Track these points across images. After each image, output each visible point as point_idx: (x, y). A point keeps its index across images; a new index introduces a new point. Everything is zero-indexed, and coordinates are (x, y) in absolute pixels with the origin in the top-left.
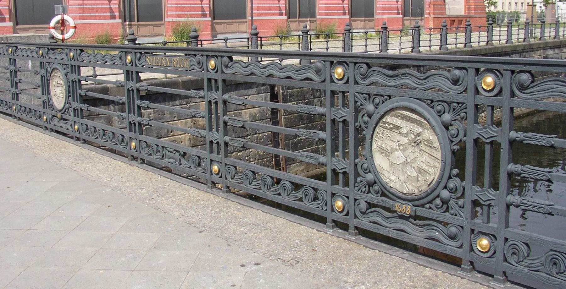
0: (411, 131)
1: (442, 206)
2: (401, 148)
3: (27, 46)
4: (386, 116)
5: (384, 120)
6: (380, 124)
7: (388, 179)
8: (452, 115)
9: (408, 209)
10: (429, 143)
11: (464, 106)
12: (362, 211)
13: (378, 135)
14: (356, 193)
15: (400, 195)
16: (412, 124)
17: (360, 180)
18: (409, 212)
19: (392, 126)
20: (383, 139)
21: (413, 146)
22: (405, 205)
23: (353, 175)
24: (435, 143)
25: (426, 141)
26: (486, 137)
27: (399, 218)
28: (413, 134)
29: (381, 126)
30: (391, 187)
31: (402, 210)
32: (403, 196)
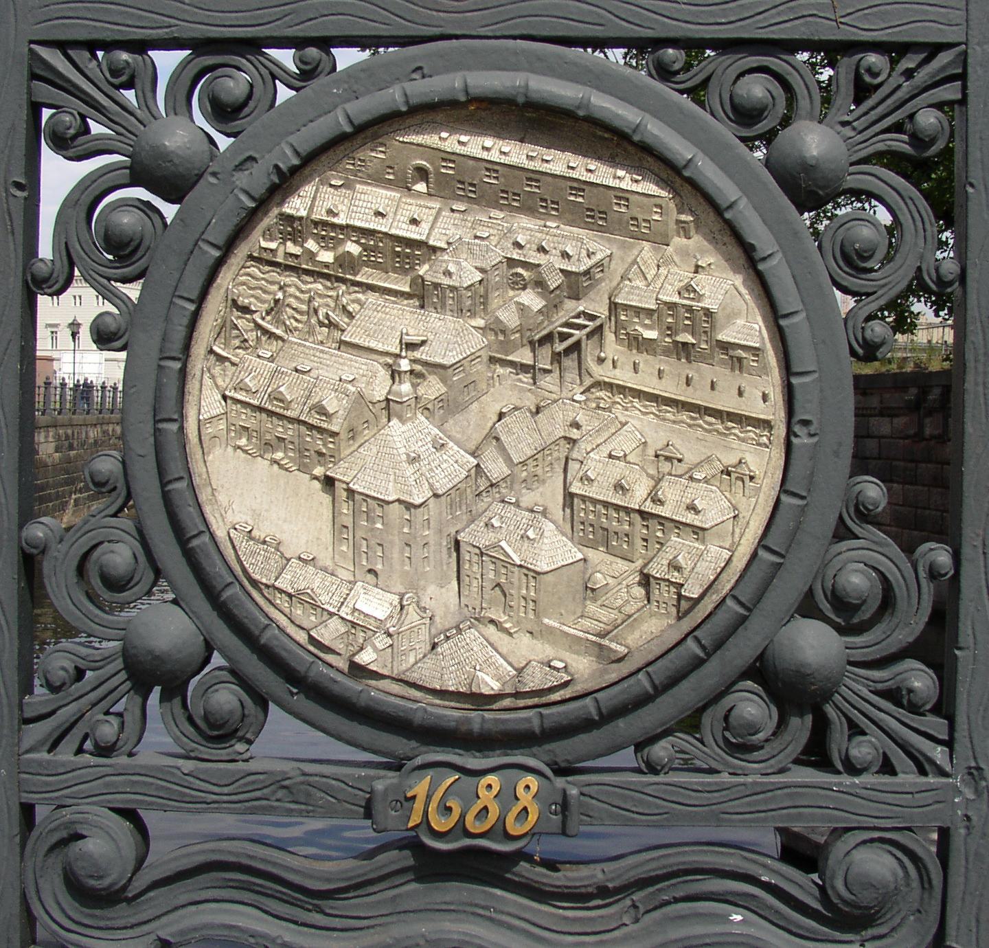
0: (511, 262)
1: (782, 723)
2: (433, 388)
3: (266, 213)
4: (306, 181)
5: (296, 206)
6: (259, 241)
7: (334, 623)
8: (848, 132)
9: (525, 798)
10: (671, 330)
11: (943, 68)
12: (106, 882)
13: (240, 323)
14: (39, 763)
15: (450, 713)
16: (525, 222)
17: (70, 666)
18: (533, 817)
19: (353, 248)
20: (275, 345)
21: (524, 368)
22: (491, 779)
23: (962, 611)
24: (732, 316)
25: (649, 312)
27: (418, 879)
28: (540, 284)
29: (264, 260)
30: (358, 671)
31: (470, 818)
32: (477, 719)
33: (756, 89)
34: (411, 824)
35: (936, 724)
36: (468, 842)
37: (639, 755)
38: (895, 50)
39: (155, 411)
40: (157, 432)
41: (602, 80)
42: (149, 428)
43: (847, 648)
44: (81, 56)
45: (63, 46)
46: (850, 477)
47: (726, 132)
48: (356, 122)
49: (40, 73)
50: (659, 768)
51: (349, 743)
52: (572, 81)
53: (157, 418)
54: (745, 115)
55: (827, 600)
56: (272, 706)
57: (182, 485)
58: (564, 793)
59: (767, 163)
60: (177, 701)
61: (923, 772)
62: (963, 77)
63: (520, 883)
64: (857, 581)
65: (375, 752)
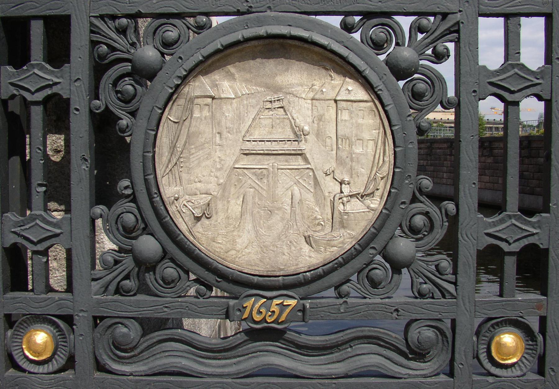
26: (35, 240)
37: (336, 291)
40: (144, 157)
41: (325, 29)
42: (141, 153)
43: (416, 247)
44: (110, 23)
45: (102, 17)
46: (417, 176)
48: (205, 55)
50: (343, 296)
52: (69, 181)
53: (146, 151)
55: (407, 227)
56: (190, 274)
61: (444, 296)
62: (458, 31)
63: (291, 341)
64: (419, 220)
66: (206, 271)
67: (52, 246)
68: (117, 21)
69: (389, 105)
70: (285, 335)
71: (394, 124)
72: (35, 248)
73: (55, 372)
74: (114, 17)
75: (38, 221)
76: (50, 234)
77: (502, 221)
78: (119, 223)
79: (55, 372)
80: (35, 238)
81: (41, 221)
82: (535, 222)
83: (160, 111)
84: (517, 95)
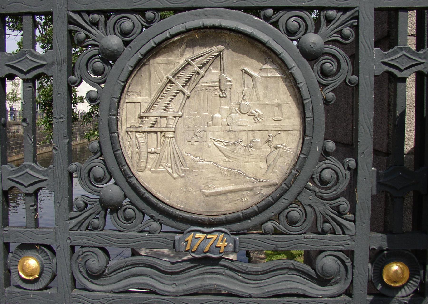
26: (25, 70)
33: (293, 24)
34: (187, 249)
35: (351, 216)
36: (205, 255)
38: (338, 9)
39: (110, 130)
44: (85, 15)
45: (79, 13)
47: (285, 37)
49: (71, 21)
51: (170, 226)
54: (290, 33)
57: (120, 152)
58: (235, 239)
59: (298, 46)
60: (115, 214)
64: (327, 174)
65: (178, 229)
66: (160, 214)
67: (41, 188)
68: (91, 16)
69: (301, 82)
70: (220, 262)
71: (306, 98)
72: (25, 77)
73: (40, 290)
74: (89, 13)
75: (27, 56)
76: (37, 65)
77: (395, 53)
78: (91, 176)
79: (40, 290)
80: (25, 69)
81: (29, 55)
82: (422, 54)
83: (123, 84)
84: (405, 72)
